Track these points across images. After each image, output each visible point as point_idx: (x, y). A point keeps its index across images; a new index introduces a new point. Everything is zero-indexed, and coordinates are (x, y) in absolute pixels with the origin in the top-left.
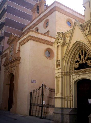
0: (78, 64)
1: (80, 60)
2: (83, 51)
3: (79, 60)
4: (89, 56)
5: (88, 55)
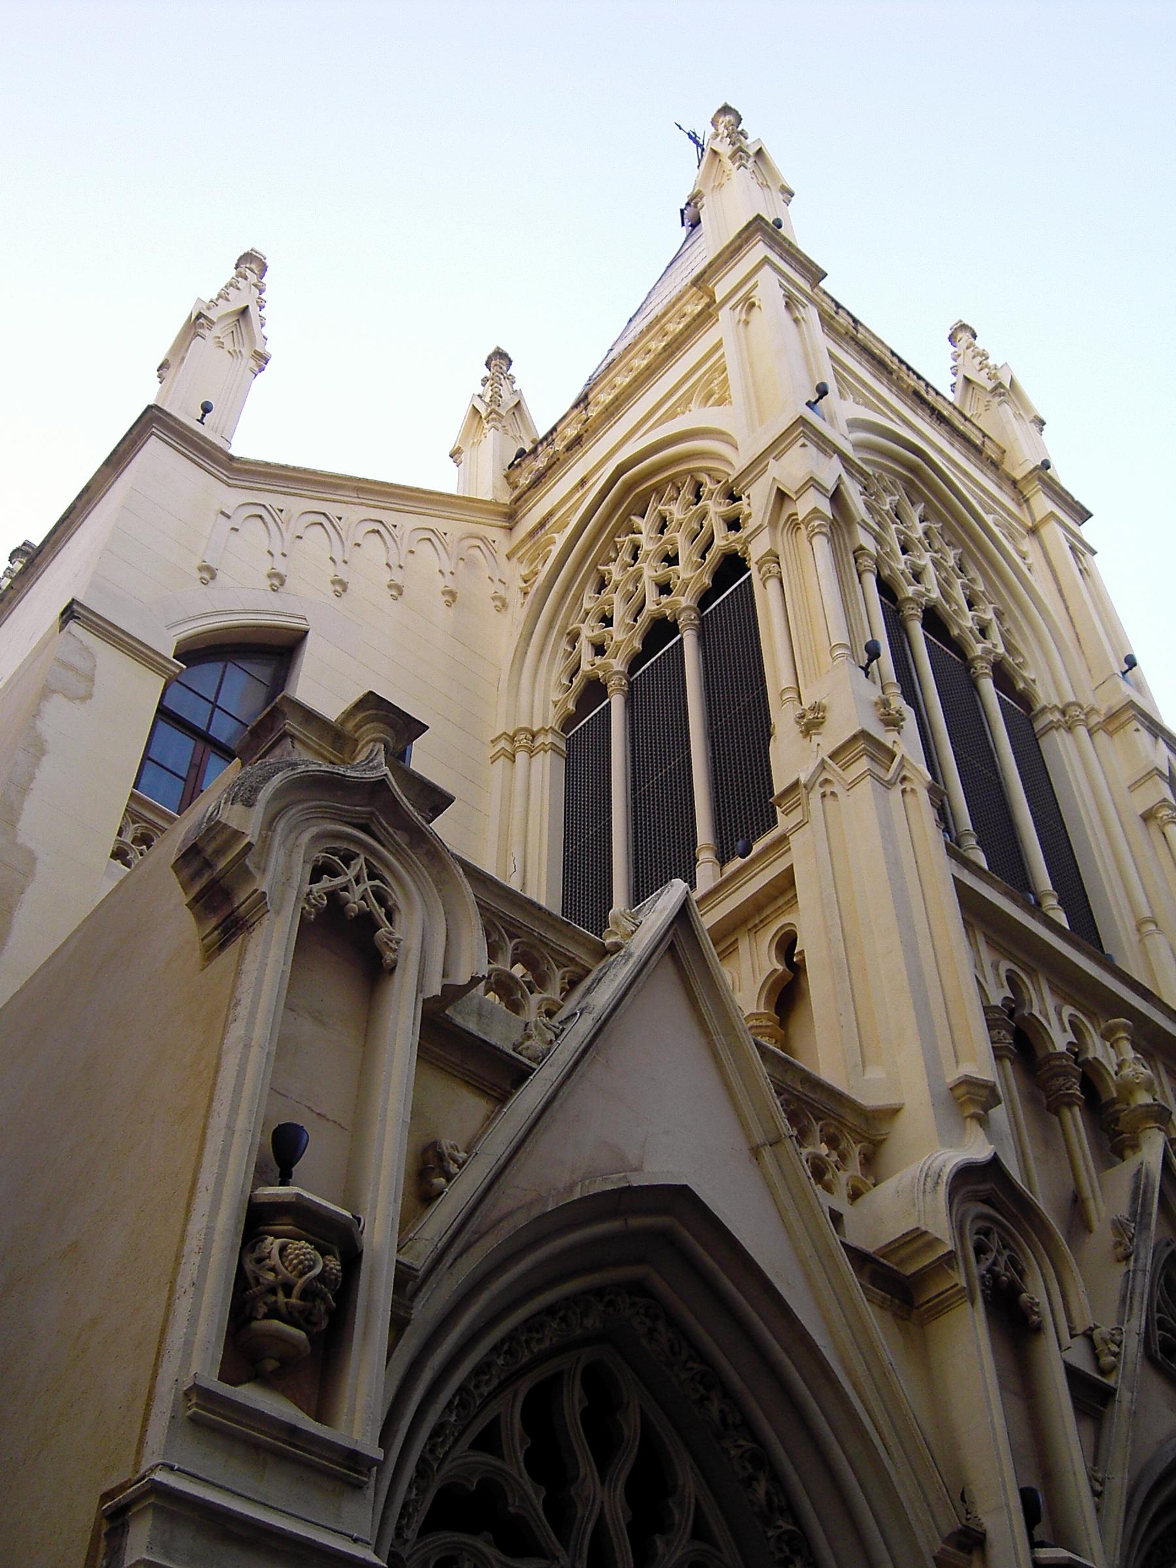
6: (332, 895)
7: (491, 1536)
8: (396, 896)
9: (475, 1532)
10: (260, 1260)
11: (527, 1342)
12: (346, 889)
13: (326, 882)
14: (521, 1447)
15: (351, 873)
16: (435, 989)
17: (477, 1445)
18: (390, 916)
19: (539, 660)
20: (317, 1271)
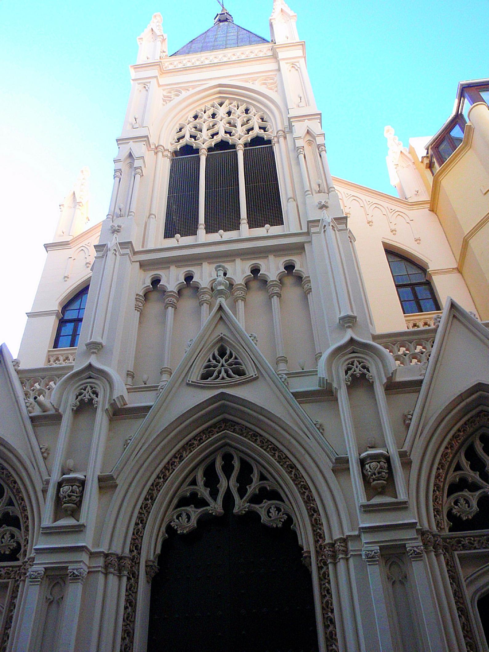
0: (195, 513)
1: (214, 494)
2: (232, 458)
3: (204, 492)
4: (10, 509)
5: (10, 503)
6: (352, 375)
7: (467, 490)
8: (368, 365)
9: (462, 491)
10: (367, 471)
11: (439, 481)
12: (355, 371)
13: (350, 373)
14: (447, 526)
15: (354, 367)
16: (385, 381)
17: (455, 470)
18: (368, 371)
19: (187, 107)
20: (379, 467)
